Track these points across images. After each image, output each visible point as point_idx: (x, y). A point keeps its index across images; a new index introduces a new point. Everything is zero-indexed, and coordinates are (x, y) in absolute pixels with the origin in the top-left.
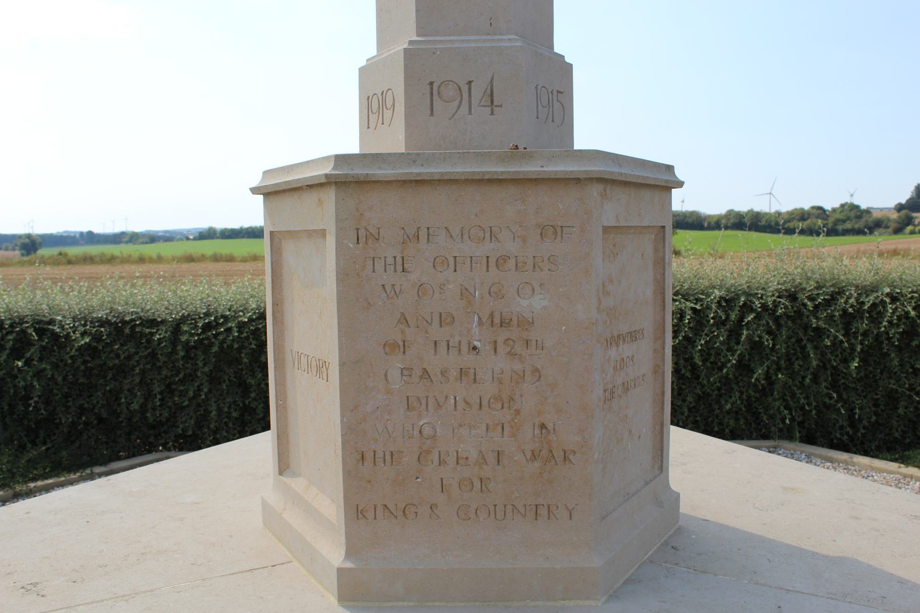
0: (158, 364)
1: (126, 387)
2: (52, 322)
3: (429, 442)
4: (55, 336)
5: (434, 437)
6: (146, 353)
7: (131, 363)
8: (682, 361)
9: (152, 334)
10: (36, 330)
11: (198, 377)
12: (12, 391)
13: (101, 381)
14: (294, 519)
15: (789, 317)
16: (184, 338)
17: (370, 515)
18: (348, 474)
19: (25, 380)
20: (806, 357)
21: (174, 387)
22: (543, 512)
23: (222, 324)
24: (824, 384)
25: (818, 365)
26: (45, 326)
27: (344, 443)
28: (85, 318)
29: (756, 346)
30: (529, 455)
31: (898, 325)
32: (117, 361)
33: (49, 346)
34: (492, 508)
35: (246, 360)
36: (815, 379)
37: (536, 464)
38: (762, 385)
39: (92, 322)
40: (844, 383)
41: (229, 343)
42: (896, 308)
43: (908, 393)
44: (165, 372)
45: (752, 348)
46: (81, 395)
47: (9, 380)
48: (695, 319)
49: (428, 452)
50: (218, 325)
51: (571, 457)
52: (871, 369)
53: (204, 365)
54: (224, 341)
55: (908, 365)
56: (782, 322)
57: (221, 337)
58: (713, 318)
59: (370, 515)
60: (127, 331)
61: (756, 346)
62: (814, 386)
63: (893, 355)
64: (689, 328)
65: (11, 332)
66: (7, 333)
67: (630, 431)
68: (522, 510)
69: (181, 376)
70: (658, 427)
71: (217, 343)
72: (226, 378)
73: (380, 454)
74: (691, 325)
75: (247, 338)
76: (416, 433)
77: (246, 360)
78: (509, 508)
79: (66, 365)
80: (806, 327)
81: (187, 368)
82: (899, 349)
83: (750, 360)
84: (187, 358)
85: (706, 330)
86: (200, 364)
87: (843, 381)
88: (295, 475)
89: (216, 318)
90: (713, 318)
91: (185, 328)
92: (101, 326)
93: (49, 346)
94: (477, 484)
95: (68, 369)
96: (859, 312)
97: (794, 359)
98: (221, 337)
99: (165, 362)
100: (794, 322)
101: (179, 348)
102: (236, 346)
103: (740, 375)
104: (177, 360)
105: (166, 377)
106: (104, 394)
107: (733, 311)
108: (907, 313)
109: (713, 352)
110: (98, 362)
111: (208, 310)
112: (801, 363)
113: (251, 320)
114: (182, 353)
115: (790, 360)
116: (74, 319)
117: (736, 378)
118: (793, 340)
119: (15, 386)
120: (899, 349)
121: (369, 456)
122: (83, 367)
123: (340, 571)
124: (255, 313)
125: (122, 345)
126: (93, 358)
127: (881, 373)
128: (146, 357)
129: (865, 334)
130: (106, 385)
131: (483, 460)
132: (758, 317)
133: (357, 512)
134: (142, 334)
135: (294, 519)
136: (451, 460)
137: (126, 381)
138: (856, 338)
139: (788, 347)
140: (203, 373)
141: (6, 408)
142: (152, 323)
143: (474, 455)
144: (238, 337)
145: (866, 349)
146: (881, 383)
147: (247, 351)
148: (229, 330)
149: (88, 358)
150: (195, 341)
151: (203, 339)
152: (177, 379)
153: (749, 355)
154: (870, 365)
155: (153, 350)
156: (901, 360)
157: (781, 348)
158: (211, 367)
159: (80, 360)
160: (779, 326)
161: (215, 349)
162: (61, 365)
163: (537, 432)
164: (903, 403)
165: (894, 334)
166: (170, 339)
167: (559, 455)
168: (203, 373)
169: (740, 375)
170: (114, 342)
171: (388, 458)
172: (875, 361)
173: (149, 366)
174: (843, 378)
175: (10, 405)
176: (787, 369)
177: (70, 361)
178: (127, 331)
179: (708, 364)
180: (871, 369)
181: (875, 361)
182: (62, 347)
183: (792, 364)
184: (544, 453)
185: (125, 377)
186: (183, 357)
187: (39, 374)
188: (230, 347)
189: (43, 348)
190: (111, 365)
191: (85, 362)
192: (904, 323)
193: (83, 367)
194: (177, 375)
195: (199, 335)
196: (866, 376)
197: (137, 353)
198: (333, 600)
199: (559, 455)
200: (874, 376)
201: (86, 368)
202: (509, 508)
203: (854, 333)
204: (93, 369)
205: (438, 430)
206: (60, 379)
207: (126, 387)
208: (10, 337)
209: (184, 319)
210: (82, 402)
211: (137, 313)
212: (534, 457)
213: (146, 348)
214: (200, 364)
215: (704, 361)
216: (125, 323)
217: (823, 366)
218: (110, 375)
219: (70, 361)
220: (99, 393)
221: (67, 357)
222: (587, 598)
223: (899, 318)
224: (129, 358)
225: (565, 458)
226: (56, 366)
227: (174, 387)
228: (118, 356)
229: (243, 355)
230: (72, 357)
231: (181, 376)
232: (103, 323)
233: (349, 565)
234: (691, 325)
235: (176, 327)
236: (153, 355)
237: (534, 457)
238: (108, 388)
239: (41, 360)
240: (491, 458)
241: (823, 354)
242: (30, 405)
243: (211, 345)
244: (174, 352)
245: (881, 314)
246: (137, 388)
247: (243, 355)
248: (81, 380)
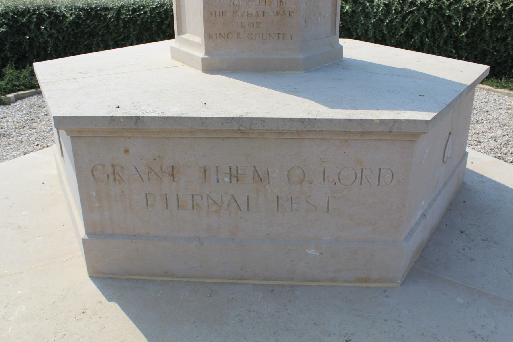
0: (110, 31)
1: (95, 43)
2: (54, 8)
3: (237, 7)
4: (57, 16)
5: (239, 5)
6: (104, 25)
7: (96, 30)
8: (377, 32)
9: (106, 15)
10: (47, 13)
11: (130, 37)
12: (38, 45)
13: (82, 40)
14: (185, 49)
15: (435, 10)
16: (123, 17)
17: (214, 37)
18: (206, 20)
19: (44, 38)
20: (442, 32)
21: (119, 43)
22: (281, 36)
23: (142, 10)
24: (450, 46)
25: (447, 36)
26: (51, 11)
27: (204, 8)
28: (71, 7)
29: (416, 25)
30: (275, 13)
31: (491, 15)
32: (89, 29)
33: (54, 21)
34: (261, 35)
35: (154, 28)
36: (446, 43)
37: (278, 17)
38: (418, 46)
39: (75, 9)
40: (460, 46)
41: (146, 19)
42: (492, 6)
43: (492, 50)
44: (114, 35)
45: (414, 26)
46: (72, 48)
47: (35, 39)
48: (385, 10)
49: (237, 11)
50: (140, 10)
51: (292, 14)
52: (475, 39)
53: (134, 31)
54: (143, 18)
55: (494, 36)
56: (431, 12)
57: (142, 16)
58: (394, 9)
59: (214, 37)
60: (93, 13)
61: (416, 25)
62: (445, 47)
63: (487, 31)
64: (382, 14)
65: (34, 14)
66: (33, 14)
67: (320, 14)
68: (273, 35)
69: (122, 37)
70: (334, 16)
71: (140, 19)
72: (145, 38)
73: (218, 13)
74: (383, 12)
75: (155, 16)
76: (232, 4)
77: (154, 28)
78: (268, 35)
79: (63, 31)
80: (443, 16)
81: (125, 33)
82: (491, 28)
83: (412, 32)
84: (124, 27)
85: (391, 15)
86: (132, 30)
87: (459, 44)
88: (184, 34)
89: (139, 6)
90: (394, 9)
91: (123, 11)
92: (80, 11)
93: (54, 21)
94: (255, 25)
95: (65, 33)
96: (471, 8)
97: (436, 32)
98: (142, 16)
99: (114, 30)
100: (437, 12)
101: (120, 22)
102: (149, 21)
103: (407, 40)
104: (120, 28)
105: (115, 37)
106: (84, 47)
107: (405, 5)
108: (497, 8)
109: (393, 27)
110: (80, 30)
111: (135, 2)
112: (439, 34)
113: (157, 7)
114: (122, 25)
115: (433, 33)
116: (66, 7)
117: (405, 42)
118: (436, 22)
119: (39, 42)
120: (491, 28)
121: (214, 13)
122: (72, 33)
123: (203, 59)
124: (159, 4)
125: (91, 21)
126: (77, 28)
127: (480, 41)
128: (104, 27)
129: (474, 19)
130: (84, 42)
131: (258, 15)
132: (419, 9)
133: (209, 36)
134: (101, 15)
135: (185, 49)
136: (245, 15)
137: (94, 40)
138: (469, 21)
139: (433, 26)
140: (133, 34)
141: (36, 53)
142: (106, 9)
143: (254, 13)
144: (150, 16)
145: (474, 27)
146: (479, 46)
147: (155, 23)
148: (145, 13)
149: (74, 28)
150: (129, 18)
151: (132, 17)
152: (120, 38)
153: (413, 30)
154: (475, 37)
155: (107, 24)
156: (491, 34)
157: (429, 26)
158: (137, 32)
159: (70, 30)
160: (429, 14)
161: (139, 22)
162: (61, 31)
163: (279, 3)
164: (489, 57)
165: (489, 19)
166: (116, 18)
167: (287, 13)
168: (133, 34)
169: (407, 40)
170: (87, 19)
171: (221, 14)
172: (478, 35)
173: (106, 32)
174: (460, 43)
175: (37, 52)
176: (431, 37)
177: (65, 29)
178: (93, 13)
179: (391, 34)
180: (475, 39)
181: (478, 35)
182: (61, 22)
183: (434, 35)
184: (282, 12)
185: (94, 38)
186: (123, 27)
187: (50, 36)
188: (147, 21)
189: (51, 22)
190: (86, 31)
191: (73, 30)
192: (495, 14)
193: (72, 33)
194: (120, 37)
195: (130, 15)
196: (473, 42)
197: (99, 25)
198: (200, 72)
199: (287, 13)
200: (476, 42)
201: (74, 33)
202: (268, 35)
203: (468, 19)
204: (77, 33)
205: (240, 3)
206: (61, 38)
207: (95, 43)
208: (34, 16)
209: (122, 7)
210: (73, 51)
211: (97, 3)
212: (277, 14)
213: (104, 23)
214: (132, 30)
215: (389, 32)
216: (91, 9)
217: (450, 36)
218: (86, 37)
219: (65, 29)
220: (81, 46)
221: (64, 27)
222: (297, 71)
223: (493, 11)
224: (95, 28)
225: (290, 15)
226: (59, 32)
227: (119, 43)
228: (90, 27)
229: (153, 26)
230: (66, 27)
231: (122, 37)
232: (82, 9)
233: (206, 57)
234: (383, 12)
235: (119, 11)
236: (108, 26)
237: (277, 14)
238: (86, 43)
239: (51, 29)
240: (261, 14)
241: (451, 30)
242: (48, 51)
243: (137, 20)
244: (118, 24)
245: (483, 9)
246: (100, 43)
247: (153, 26)
248: (72, 39)
